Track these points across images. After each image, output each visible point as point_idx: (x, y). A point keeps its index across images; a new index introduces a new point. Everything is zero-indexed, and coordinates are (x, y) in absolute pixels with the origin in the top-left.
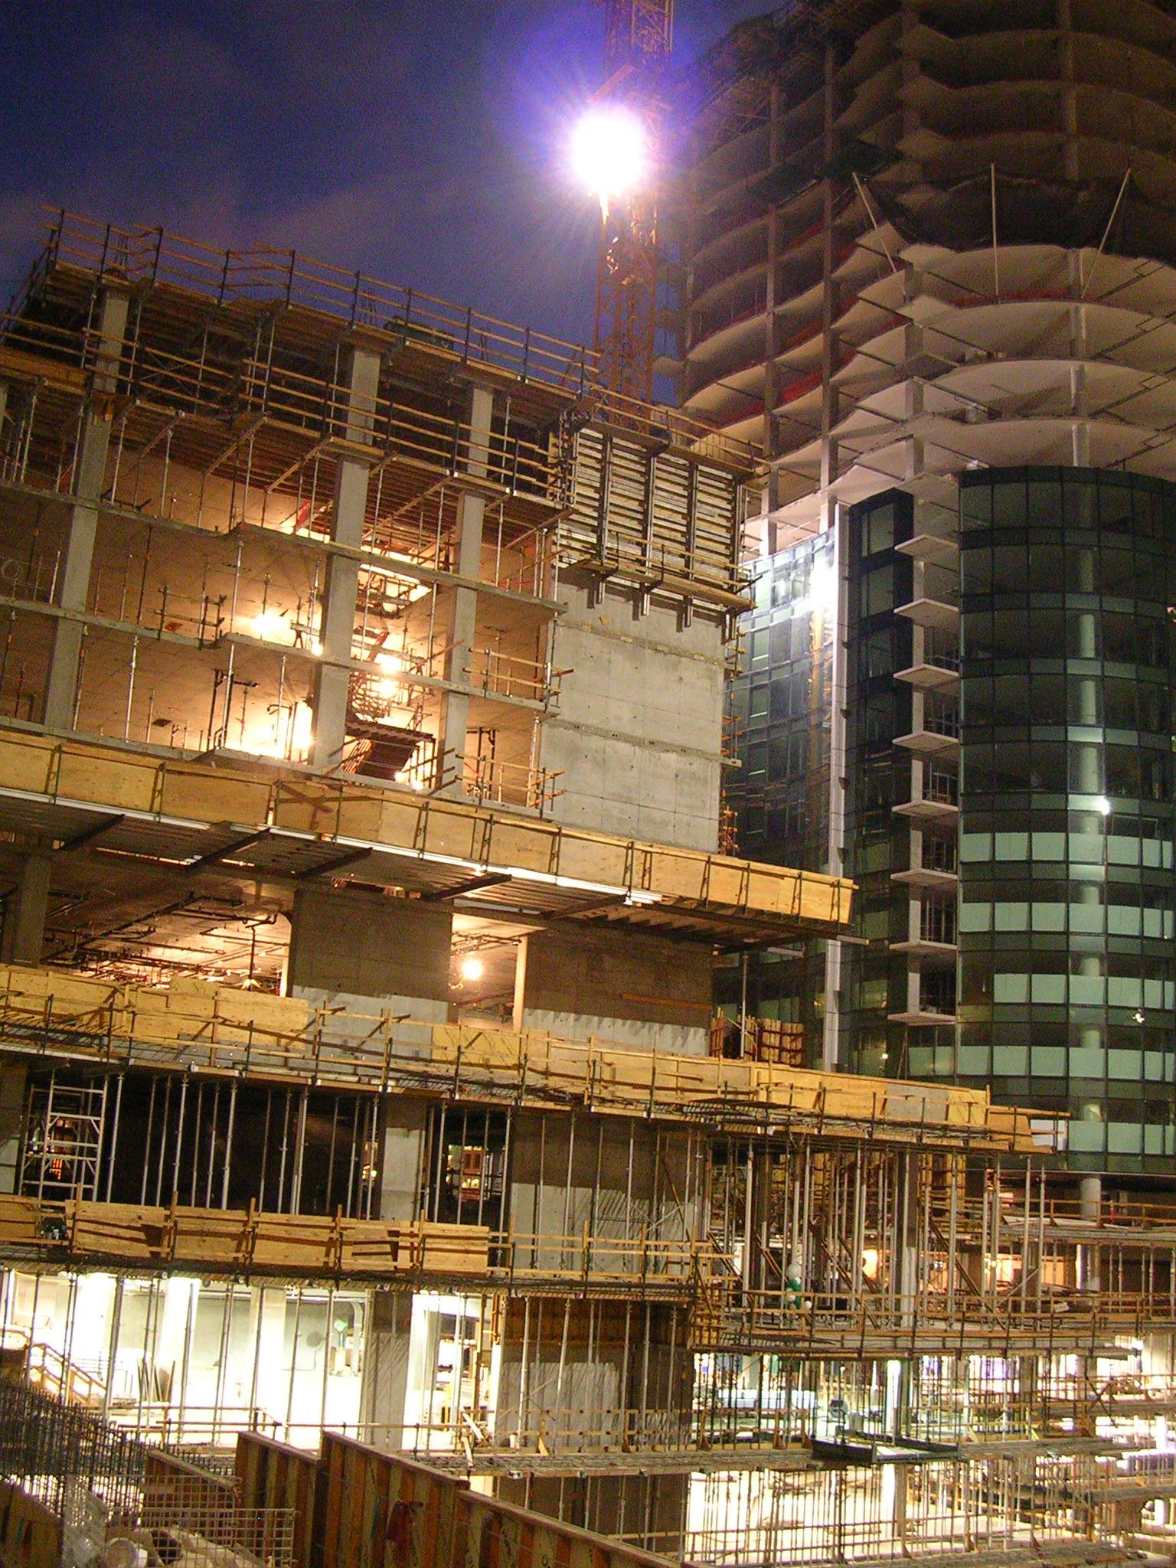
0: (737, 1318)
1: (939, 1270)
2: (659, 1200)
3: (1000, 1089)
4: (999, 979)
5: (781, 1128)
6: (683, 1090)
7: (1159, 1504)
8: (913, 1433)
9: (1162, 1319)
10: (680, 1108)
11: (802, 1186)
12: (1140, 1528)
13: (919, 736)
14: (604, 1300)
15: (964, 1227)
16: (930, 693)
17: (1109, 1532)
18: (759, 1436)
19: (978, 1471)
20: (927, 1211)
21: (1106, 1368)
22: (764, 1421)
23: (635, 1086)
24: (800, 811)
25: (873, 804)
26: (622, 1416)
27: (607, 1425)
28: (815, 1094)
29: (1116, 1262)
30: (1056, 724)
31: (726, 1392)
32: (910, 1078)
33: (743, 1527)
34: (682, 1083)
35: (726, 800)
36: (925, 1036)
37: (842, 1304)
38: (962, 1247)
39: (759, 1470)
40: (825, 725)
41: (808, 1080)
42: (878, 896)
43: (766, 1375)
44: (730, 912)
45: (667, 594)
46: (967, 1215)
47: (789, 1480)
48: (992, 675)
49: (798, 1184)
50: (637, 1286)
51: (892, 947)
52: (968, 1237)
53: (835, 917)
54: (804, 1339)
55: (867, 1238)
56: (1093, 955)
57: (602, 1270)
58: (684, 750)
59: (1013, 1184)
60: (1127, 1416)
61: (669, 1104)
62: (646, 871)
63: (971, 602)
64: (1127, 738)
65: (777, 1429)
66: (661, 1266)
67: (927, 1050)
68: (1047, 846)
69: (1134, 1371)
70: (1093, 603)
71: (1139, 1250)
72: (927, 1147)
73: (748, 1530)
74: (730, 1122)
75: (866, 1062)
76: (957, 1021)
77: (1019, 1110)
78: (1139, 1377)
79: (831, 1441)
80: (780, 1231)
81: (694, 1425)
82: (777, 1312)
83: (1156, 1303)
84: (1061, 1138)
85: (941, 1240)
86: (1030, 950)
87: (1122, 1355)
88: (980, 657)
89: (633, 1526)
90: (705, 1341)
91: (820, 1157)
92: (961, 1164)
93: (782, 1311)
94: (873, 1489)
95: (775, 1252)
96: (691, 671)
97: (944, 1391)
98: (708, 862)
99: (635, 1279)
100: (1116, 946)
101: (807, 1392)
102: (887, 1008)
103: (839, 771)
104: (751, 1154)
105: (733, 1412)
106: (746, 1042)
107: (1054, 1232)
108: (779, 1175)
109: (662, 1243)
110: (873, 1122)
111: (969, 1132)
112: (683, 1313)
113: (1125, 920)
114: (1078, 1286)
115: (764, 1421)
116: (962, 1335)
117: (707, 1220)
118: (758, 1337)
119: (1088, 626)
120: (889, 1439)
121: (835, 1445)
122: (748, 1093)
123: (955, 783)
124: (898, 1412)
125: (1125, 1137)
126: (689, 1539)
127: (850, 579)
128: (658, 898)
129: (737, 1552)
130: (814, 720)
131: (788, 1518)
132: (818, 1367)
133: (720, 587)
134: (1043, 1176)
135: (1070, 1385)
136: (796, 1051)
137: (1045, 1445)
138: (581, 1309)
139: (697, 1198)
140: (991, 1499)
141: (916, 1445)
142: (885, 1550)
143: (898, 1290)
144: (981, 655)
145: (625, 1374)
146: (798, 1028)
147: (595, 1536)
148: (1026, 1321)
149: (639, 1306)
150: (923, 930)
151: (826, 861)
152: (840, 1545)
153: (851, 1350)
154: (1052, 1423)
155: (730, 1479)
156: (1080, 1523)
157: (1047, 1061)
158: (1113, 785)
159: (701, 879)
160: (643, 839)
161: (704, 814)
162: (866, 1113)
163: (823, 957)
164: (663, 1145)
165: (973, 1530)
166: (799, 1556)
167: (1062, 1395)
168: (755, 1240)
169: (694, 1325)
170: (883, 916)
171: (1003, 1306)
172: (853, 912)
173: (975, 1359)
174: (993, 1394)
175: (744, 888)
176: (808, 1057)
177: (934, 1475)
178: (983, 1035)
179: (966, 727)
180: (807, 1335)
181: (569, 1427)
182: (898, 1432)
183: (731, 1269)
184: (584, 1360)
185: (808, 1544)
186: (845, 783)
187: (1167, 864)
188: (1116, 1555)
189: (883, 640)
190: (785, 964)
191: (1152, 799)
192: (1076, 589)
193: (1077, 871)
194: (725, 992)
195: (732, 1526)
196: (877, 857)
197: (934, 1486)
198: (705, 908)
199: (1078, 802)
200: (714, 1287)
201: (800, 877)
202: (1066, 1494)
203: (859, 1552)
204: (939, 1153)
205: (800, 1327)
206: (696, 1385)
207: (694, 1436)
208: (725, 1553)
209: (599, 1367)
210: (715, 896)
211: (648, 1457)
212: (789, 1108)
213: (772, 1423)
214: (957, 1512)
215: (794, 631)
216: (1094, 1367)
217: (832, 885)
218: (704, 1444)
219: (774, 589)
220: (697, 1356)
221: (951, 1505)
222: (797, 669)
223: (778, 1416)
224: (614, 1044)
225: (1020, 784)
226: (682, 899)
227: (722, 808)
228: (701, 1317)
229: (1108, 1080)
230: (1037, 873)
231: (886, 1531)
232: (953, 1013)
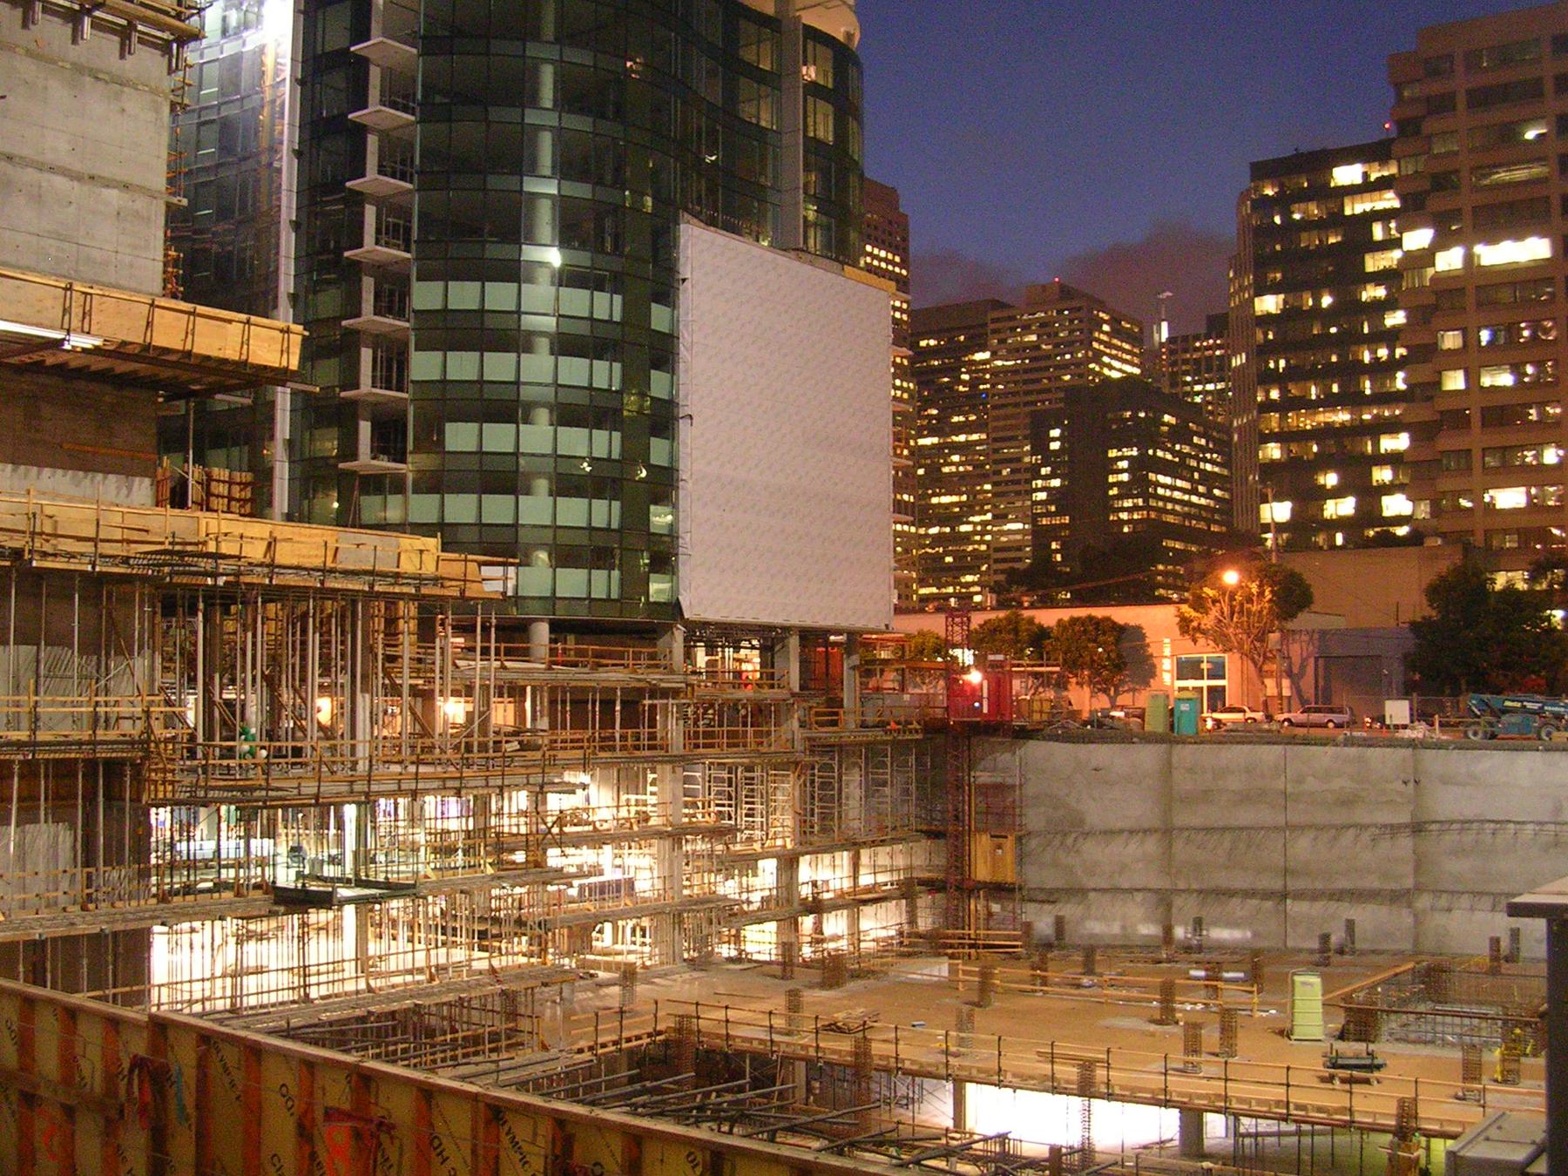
0: (193, 770)
1: (393, 715)
2: (108, 655)
3: (451, 537)
4: (450, 428)
5: (231, 578)
6: (129, 542)
7: (608, 927)
8: (372, 873)
9: (608, 754)
10: (126, 560)
11: (254, 636)
12: (591, 950)
13: (372, 180)
14: (56, 761)
15: (416, 672)
16: (384, 136)
17: (562, 956)
18: (220, 886)
19: (437, 905)
20: (380, 657)
21: (555, 802)
22: (224, 871)
23: (79, 539)
24: (249, 253)
25: (324, 249)
26: (79, 877)
27: (64, 885)
28: (265, 544)
29: (564, 702)
30: (511, 173)
31: (184, 844)
32: (362, 527)
33: (208, 975)
34: (128, 535)
35: (170, 241)
36: (376, 484)
37: (297, 752)
38: (415, 692)
39: (222, 919)
40: (276, 165)
41: (258, 529)
42: (328, 344)
43: (224, 825)
44: (174, 358)
45: (110, 18)
46: (420, 661)
47: (252, 927)
48: (450, 120)
49: (250, 635)
50: (88, 743)
51: (343, 394)
52: (421, 682)
53: (284, 364)
54: (260, 788)
55: (321, 686)
56: (543, 405)
57: (51, 729)
58: (126, 187)
59: (464, 629)
60: (576, 846)
61: (114, 557)
62: (86, 314)
63: (430, 44)
64: (582, 190)
65: (237, 877)
66: (113, 721)
67: (377, 499)
68: (499, 295)
69: (581, 803)
70: (553, 52)
71: (584, 690)
72: (379, 594)
73: (213, 978)
74: (178, 573)
75: (317, 509)
76: (408, 469)
77: (470, 557)
78: (586, 810)
79: (292, 886)
80: (233, 682)
81: (154, 880)
82: (232, 763)
83: (603, 739)
84: (511, 584)
85: (394, 685)
86: (482, 400)
87: (570, 789)
88: (437, 101)
89: (97, 983)
90: (161, 795)
91: (271, 606)
92: (413, 612)
93: (237, 761)
94: (336, 930)
95: (229, 704)
96: (134, 103)
97: (401, 831)
98: (152, 305)
99: (85, 735)
100: (564, 397)
101: (266, 840)
102: (337, 456)
103: (289, 214)
104: (201, 606)
105: (192, 864)
106: (194, 491)
107: (504, 675)
108: (230, 626)
109: (112, 699)
110: (326, 571)
111: (420, 579)
112: (137, 770)
113: (575, 371)
114: (529, 725)
115: (224, 871)
116: (417, 777)
117: (158, 674)
118: (214, 788)
119: (547, 75)
120: (349, 881)
121: (296, 889)
122: (196, 544)
123: (408, 230)
124: (356, 854)
125: (572, 582)
126: (155, 992)
127: (305, 13)
128: (98, 342)
129: (203, 1000)
130: (264, 159)
131: (252, 964)
132: (276, 814)
133: (167, 13)
134: (494, 621)
135: (523, 820)
136: (245, 501)
137: (499, 878)
138: (30, 771)
139: (147, 652)
140: (449, 931)
141: (376, 885)
142: (350, 986)
143: (353, 736)
144: (438, 99)
145: (80, 832)
146: (247, 477)
147: (59, 995)
148: (479, 760)
149: (91, 764)
150: (374, 377)
151: (275, 307)
152: (305, 986)
153: (309, 797)
154: (505, 856)
155: (193, 930)
156: (535, 948)
157: (497, 509)
158: (567, 236)
159: (144, 323)
160: (83, 281)
161: (147, 254)
162: (318, 562)
163: (272, 404)
164: (109, 598)
165: (433, 962)
166: (265, 999)
167: (514, 830)
168: (208, 692)
169: (149, 780)
170: (333, 363)
171: (457, 748)
172: (303, 359)
173: (429, 799)
174: (449, 832)
175: (190, 332)
176: (258, 506)
177: (394, 913)
178: (434, 484)
179: (421, 173)
180: (263, 783)
181: (24, 889)
182: (357, 874)
183: (184, 721)
184: (36, 821)
185: (273, 987)
186: (296, 226)
187: (617, 317)
188: (571, 976)
189: (338, 79)
190: (233, 412)
191: (603, 251)
192: (536, 36)
193: (529, 322)
194: (171, 440)
195: (197, 975)
196: (328, 301)
197: (394, 923)
198: (149, 353)
199: (530, 253)
200: (167, 741)
201: (248, 322)
202: (520, 922)
203: (324, 991)
204: (392, 600)
205: (257, 777)
206: (153, 839)
207: (154, 890)
208: (191, 1002)
209: (52, 827)
210: (160, 340)
211: (107, 914)
212: (239, 558)
213: (232, 873)
214: (417, 946)
215: (245, 65)
216: (545, 802)
217: (282, 331)
218: (163, 897)
219: (224, 19)
220: (153, 810)
221: (411, 940)
222: (248, 105)
223: (238, 865)
224: (56, 495)
225: (476, 235)
226: (124, 343)
227: (166, 249)
228: (155, 771)
229: (556, 528)
230: (490, 322)
231: (350, 969)
232: (403, 461)
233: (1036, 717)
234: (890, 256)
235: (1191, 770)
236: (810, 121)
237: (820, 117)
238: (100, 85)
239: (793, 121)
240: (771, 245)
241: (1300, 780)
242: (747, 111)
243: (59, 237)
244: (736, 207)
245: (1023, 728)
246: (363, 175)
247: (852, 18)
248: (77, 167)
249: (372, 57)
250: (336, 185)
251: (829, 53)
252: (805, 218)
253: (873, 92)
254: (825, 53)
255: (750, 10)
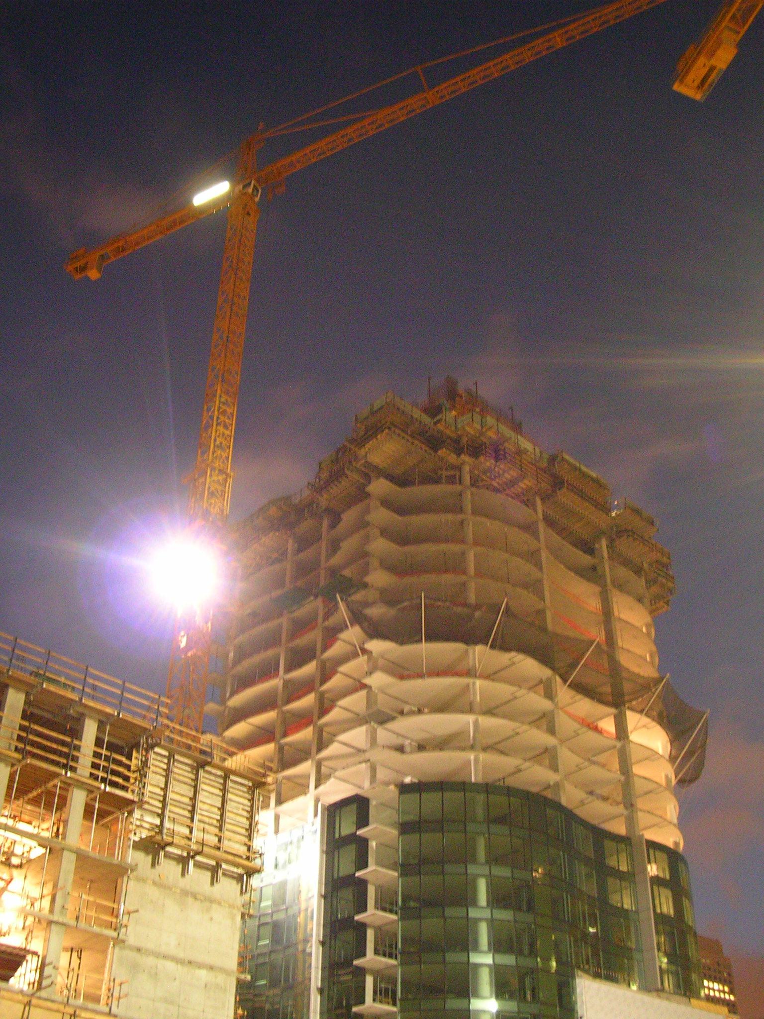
13: (370, 959)
16: (378, 930)
25: (339, 1006)
58: (211, 968)
63: (406, 869)
64: (509, 960)
70: (485, 870)
88: (412, 906)
96: (218, 913)
119: (482, 886)
123: (394, 992)
130: (300, 947)
133: (241, 857)
144: (412, 904)
192: (474, 861)
215: (289, 887)
222: (291, 912)
234: (721, 987)
236: (657, 902)
237: (663, 900)
238: (198, 903)
239: (644, 902)
240: (639, 988)
242: (614, 899)
243: (166, 1000)
244: (612, 964)
246: (367, 867)
247: (678, 832)
248: (181, 955)
249: (369, 878)
250: (348, 963)
251: (665, 856)
252: (660, 967)
253: (695, 877)
254: (662, 856)
255: (610, 833)
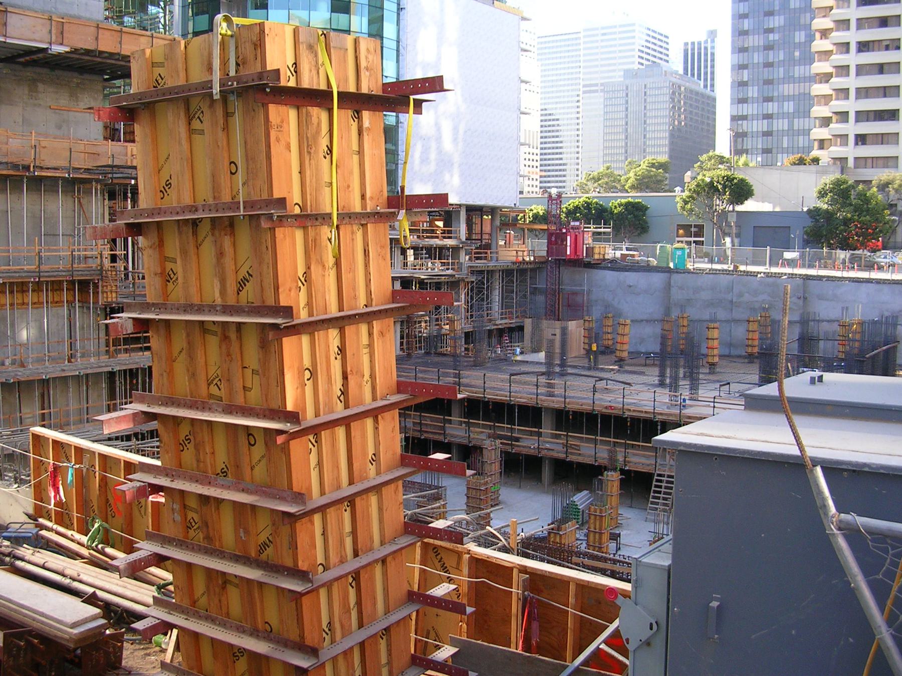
104: (129, 195)
112: (96, 286)
128: (68, 49)
233: (596, 257)
235: (681, 288)
241: (740, 295)
245: (589, 263)
